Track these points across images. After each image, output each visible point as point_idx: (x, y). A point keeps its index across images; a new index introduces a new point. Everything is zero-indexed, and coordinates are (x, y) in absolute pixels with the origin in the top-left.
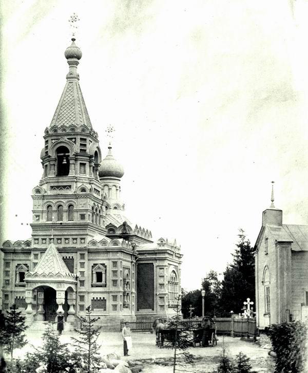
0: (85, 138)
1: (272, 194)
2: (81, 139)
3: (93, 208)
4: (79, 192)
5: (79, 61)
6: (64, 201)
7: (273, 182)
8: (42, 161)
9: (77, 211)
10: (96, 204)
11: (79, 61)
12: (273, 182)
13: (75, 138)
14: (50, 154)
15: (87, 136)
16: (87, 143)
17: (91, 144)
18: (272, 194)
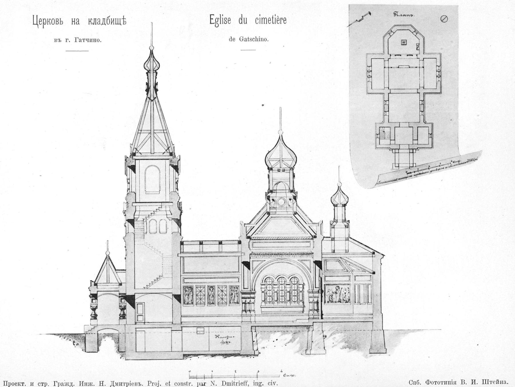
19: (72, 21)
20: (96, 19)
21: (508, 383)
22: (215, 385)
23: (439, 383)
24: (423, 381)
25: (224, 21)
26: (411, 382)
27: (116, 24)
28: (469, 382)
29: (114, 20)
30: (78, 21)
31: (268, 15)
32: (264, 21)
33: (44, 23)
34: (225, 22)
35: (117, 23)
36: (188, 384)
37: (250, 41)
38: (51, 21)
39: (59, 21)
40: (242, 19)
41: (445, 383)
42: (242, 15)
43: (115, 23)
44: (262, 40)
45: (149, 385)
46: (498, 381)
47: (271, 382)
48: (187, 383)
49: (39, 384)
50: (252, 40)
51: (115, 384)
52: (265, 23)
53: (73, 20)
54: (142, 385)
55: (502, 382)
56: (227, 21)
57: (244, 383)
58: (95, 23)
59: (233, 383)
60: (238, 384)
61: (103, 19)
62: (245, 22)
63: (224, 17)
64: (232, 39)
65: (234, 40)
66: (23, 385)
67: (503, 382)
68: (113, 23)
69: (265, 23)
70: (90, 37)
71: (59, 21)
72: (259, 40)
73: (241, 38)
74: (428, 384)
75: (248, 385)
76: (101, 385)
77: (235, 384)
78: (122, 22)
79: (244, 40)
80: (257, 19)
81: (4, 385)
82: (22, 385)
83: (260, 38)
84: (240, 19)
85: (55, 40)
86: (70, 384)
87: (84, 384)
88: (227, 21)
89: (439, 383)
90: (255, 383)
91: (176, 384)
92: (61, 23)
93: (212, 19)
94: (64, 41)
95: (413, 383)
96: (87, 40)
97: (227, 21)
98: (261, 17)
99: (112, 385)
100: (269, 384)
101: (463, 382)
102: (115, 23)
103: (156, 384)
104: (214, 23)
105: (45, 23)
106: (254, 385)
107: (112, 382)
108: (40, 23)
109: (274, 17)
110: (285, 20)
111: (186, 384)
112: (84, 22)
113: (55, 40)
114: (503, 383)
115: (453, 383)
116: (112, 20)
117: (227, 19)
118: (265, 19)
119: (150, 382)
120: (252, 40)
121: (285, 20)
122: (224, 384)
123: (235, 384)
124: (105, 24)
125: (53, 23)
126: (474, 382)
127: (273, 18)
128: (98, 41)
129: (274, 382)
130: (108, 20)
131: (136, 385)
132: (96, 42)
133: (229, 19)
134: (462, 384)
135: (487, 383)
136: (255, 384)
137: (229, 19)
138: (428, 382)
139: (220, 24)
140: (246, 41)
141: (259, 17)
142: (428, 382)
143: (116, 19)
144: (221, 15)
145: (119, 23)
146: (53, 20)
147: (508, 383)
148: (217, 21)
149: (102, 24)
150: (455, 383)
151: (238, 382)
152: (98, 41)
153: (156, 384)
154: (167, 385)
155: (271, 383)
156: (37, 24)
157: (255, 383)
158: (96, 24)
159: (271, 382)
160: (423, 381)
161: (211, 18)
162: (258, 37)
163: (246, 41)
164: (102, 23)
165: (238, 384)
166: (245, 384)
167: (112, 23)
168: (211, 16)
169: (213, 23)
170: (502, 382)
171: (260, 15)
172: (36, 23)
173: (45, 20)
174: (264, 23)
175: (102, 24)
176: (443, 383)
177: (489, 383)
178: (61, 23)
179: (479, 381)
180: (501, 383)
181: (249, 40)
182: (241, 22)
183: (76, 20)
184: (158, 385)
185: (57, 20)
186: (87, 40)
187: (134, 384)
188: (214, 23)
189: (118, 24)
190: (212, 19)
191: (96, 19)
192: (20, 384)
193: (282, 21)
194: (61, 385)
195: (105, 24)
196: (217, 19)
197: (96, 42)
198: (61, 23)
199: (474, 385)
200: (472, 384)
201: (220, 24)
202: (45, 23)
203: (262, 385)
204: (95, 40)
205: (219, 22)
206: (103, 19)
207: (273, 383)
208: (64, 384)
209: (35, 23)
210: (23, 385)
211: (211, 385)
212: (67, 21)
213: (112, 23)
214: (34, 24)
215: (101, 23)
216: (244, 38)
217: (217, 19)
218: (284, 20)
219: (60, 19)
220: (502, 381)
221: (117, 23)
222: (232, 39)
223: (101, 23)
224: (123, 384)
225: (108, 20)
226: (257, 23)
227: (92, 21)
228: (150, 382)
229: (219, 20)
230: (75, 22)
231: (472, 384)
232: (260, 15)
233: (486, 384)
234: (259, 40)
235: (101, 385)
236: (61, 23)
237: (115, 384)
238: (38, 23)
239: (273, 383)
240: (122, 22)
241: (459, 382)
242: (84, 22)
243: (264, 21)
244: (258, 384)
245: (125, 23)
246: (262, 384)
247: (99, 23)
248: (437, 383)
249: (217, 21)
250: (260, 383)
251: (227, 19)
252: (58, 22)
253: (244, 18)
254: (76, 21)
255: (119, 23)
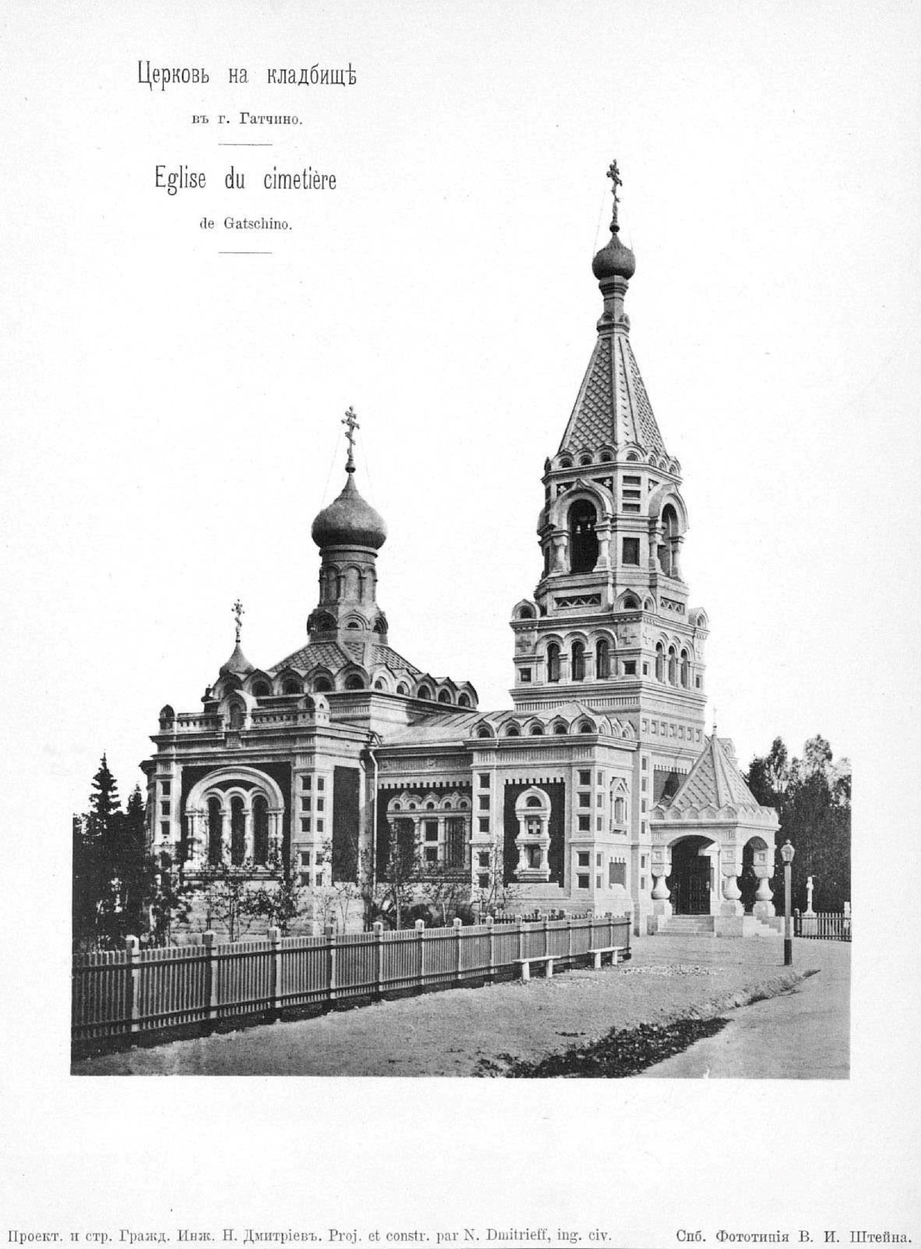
0: (635, 474)
1: (615, 218)
2: (627, 479)
3: (659, 646)
4: (621, 609)
5: (625, 281)
6: (562, 634)
7: (768, 354)
8: (539, 538)
9: (616, 655)
10: (670, 634)
11: (625, 281)
12: (768, 354)
13: (611, 478)
14: (554, 521)
15: (643, 469)
16: (643, 488)
17: (656, 489)
18: (615, 218)
19: (231, 75)
20: (285, 71)
21: (704, 1240)
22: (475, 1238)
23: (747, 1239)
24: (709, 1234)
25: (189, 180)
26: (682, 1235)
27: (332, 83)
28: (818, 1236)
29: (327, 74)
30: (245, 75)
31: (292, 168)
32: (283, 181)
33: (164, 79)
34: (193, 184)
35: (335, 81)
36: (419, 1236)
37: (248, 229)
38: (180, 74)
39: (200, 76)
40: (232, 178)
41: (763, 1238)
42: (232, 167)
43: (330, 81)
44: (278, 226)
45: (122, 1240)
46: (886, 1236)
47: (595, 1232)
48: (416, 1234)
49: (89, 1237)
50: (253, 225)
51: (254, 1237)
52: (287, 186)
53: (233, 73)
54: (318, 1239)
55: (896, 1239)
56: (197, 181)
57: (539, 1233)
58: (283, 81)
59: (514, 1234)
60: (524, 1236)
61: (302, 70)
62: (240, 185)
63: (189, 172)
64: (206, 224)
65: (211, 226)
66: (55, 1240)
67: (900, 1239)
68: (325, 81)
69: (287, 186)
70: (273, 113)
71: (200, 76)
72: (269, 226)
73: (229, 221)
74: (722, 1240)
75: (549, 1239)
76: (228, 1237)
77: (518, 1236)
78: (346, 79)
79: (235, 226)
80: (268, 177)
81: (853, 1241)
82: (52, 1238)
83: (273, 221)
84: (229, 177)
85: (195, 119)
86: (158, 1237)
87: (189, 1237)
88: (197, 181)
89: (747, 1239)
90: (562, 1235)
91: (390, 1237)
92: (205, 79)
93: (161, 176)
94: (214, 120)
95: (687, 1236)
96: (269, 119)
97: (197, 181)
98: (277, 173)
99: (249, 1238)
100: (592, 1236)
101: (804, 1236)
102: (330, 81)
103: (349, 1237)
104: (164, 186)
105: (167, 80)
106: (10, 1240)
107: (249, 1232)
108: (157, 79)
109: (308, 173)
110: (332, 180)
111: (414, 1236)
112: (258, 76)
113: (195, 119)
114: (899, 1240)
115: (781, 1238)
116: (324, 73)
117: (198, 176)
118: (288, 178)
119: (334, 1233)
120: (253, 225)
121: (332, 180)
122: (492, 1236)
123: (518, 1236)
124: (308, 83)
125: (186, 79)
126: (829, 1236)
127: (305, 175)
128: (295, 120)
129: (602, 1234)
130: (314, 73)
131: (305, 1238)
132: (289, 123)
133: (202, 177)
134: (802, 1240)
135: (861, 1239)
136: (562, 1237)
137: (202, 177)
138: (722, 1236)
139: (181, 187)
140: (239, 226)
141: (272, 173)
142: (722, 1236)
143: (332, 71)
144: (184, 168)
145: (339, 81)
146: (186, 73)
147: (704, 1240)
148: (172, 180)
149: (300, 83)
150: (786, 1238)
151: (526, 1231)
152: (295, 120)
153: (349, 1237)
154: (372, 1238)
155: (596, 1235)
156: (148, 82)
157: (562, 1235)
158: (285, 82)
159: (595, 1232)
160: (709, 1234)
161: (159, 174)
162: (267, 219)
163: (241, 227)
164: (299, 80)
165: (524, 1236)
166: (541, 1237)
167: (322, 80)
168: (159, 168)
169: (163, 184)
170: (896, 1239)
171: (275, 168)
172: (146, 80)
173: (166, 72)
174: (285, 188)
175: (300, 83)
176: (758, 1239)
177: (867, 1239)
178: (205, 79)
179: (843, 1235)
180: (896, 1240)
181: (247, 224)
182: (229, 184)
183: (238, 72)
184: (573, 1237)
185: (196, 73)
186: (269, 119)
187: (43, 1236)
188: (164, 186)
189: (337, 83)
190: (161, 176)
191: (285, 71)
192: (49, 1237)
193: (326, 183)
194: (446, 1239)
195: (308, 83)
196: (172, 177)
197: (289, 123)
198: (205, 80)
199: (830, 1244)
200: (827, 1241)
201: (181, 187)
202: (167, 80)
203: (578, 1239)
204: (287, 120)
205: (177, 184)
206: (302, 70)
207: (600, 1236)
208: (145, 1237)
209: (144, 78)
210: (55, 1240)
211: (466, 1239)
212: (219, 75)
213: (322, 80)
214: (140, 82)
215: (298, 79)
216: (235, 221)
217: (172, 177)
218: (330, 181)
219: (203, 69)
220: (898, 1236)
221: (335, 81)
222: (206, 224)
223: (298, 79)
224: (273, 1238)
225: (314, 73)
226: (268, 185)
227: (278, 75)
228: (334, 1233)
229: (178, 179)
230: (237, 76)
231: (827, 1241)
232: (275, 168)
233: (858, 1241)
234: (269, 226)
235: (228, 1237)
236: (205, 80)
237: (254, 1237)
238: (151, 80)
239: (600, 1236)
240: (346, 79)
241: (795, 1237)
242: (258, 76)
243: (283, 181)
244: (570, 1237)
245: (353, 81)
246: (577, 1237)
247: (292, 80)
248: (742, 1239)
249: (172, 180)
250: (573, 1235)
251: (198, 176)
252: (201, 77)
253: (238, 175)
254: (239, 75)
255: (339, 81)
